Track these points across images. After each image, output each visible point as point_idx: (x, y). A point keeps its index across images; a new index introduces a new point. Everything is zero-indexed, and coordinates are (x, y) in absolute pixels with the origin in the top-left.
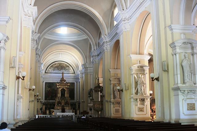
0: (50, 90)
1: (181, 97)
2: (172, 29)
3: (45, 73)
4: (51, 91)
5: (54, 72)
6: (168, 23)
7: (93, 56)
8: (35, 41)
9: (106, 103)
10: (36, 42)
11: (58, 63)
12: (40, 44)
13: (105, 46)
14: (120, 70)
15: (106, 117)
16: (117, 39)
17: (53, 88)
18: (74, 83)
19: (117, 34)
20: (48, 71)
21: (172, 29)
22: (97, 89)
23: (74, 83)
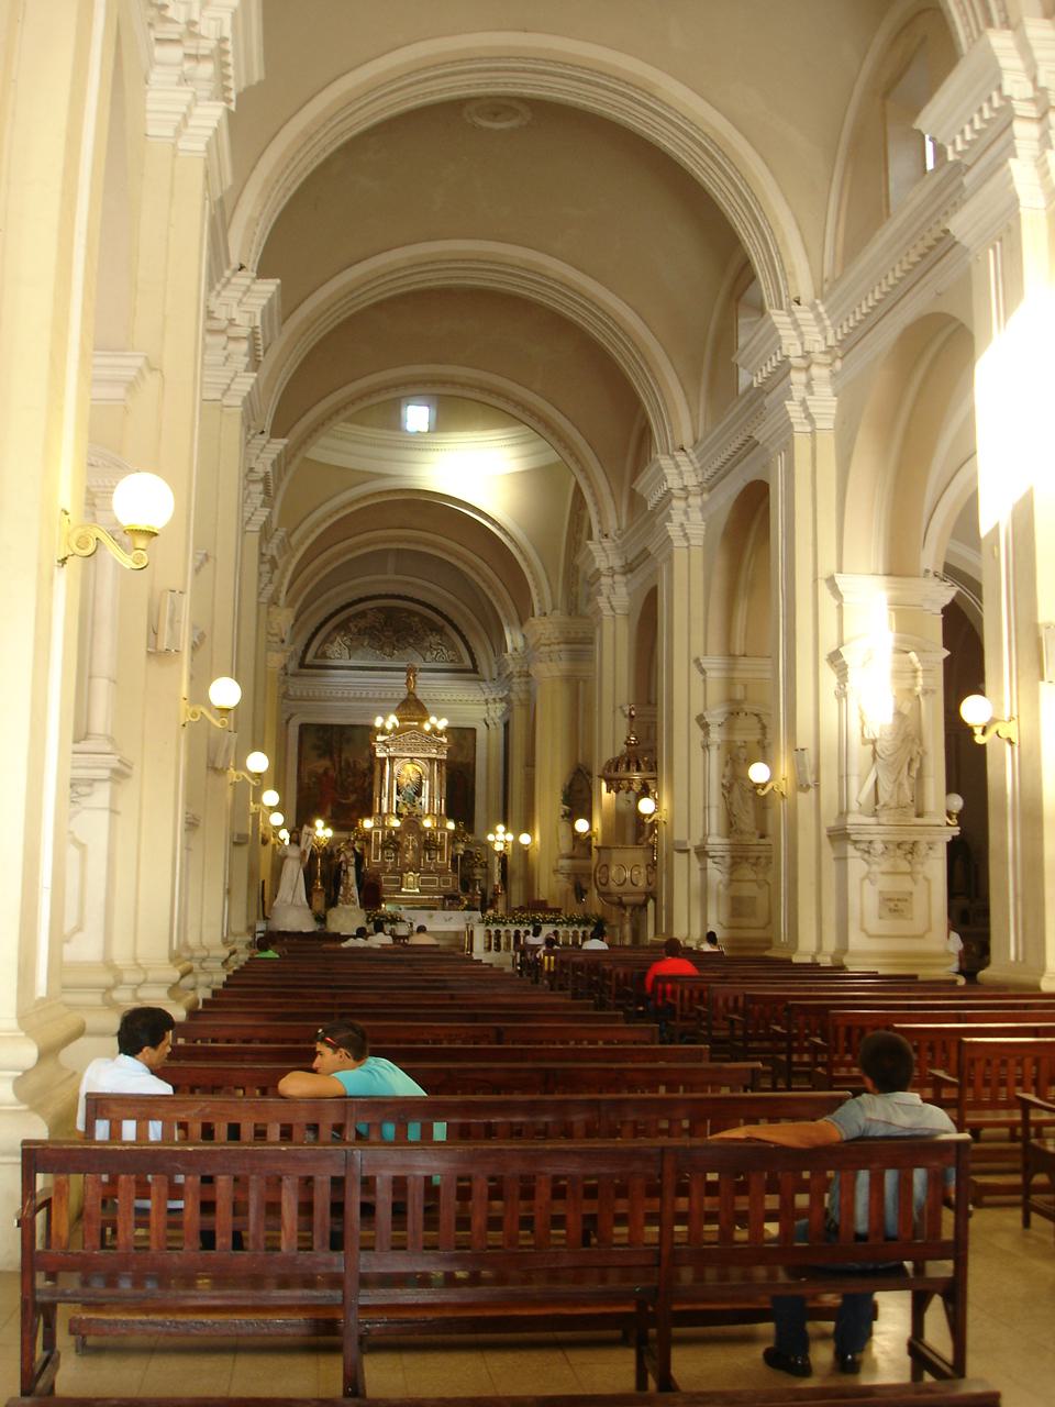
0: (326, 773)
1: (856, 866)
2: (703, 671)
3: (302, 665)
4: (332, 773)
5: (352, 663)
6: (697, 651)
7: (511, 673)
8: (236, 339)
9: (679, 861)
10: (260, 487)
11: (380, 609)
12: (281, 494)
13: (677, 517)
14: (769, 661)
15: (796, 959)
16: (750, 477)
17: (343, 756)
18: (474, 730)
19: (750, 445)
20: (316, 657)
21: (703, 671)
22: (622, 772)
23: (474, 730)
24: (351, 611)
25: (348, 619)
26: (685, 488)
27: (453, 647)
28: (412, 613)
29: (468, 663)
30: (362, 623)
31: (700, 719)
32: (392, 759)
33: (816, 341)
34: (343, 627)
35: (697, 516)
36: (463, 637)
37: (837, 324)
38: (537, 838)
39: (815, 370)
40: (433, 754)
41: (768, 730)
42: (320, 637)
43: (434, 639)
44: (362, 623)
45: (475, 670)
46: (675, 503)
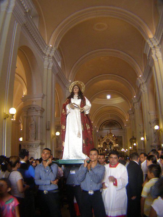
2: (150, 114)
5: (106, 129)
25: (105, 123)
26: (142, 83)
29: (121, 128)
30: (107, 124)
31: (140, 132)
33: (156, 44)
34: (104, 124)
35: (138, 106)
36: (120, 125)
37: (158, 40)
38: (137, 144)
39: (144, 85)
42: (101, 126)
43: (116, 125)
44: (107, 124)
45: (122, 129)
46: (142, 86)
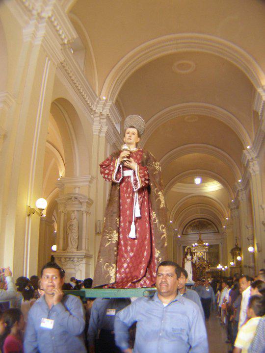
24: (191, 223)
25: (191, 224)
27: (214, 228)
28: (204, 221)
29: (217, 231)
32: (196, 252)
36: (215, 225)
40: (205, 250)
41: (65, 310)
43: (210, 226)
45: (219, 232)
46: (240, 193)
